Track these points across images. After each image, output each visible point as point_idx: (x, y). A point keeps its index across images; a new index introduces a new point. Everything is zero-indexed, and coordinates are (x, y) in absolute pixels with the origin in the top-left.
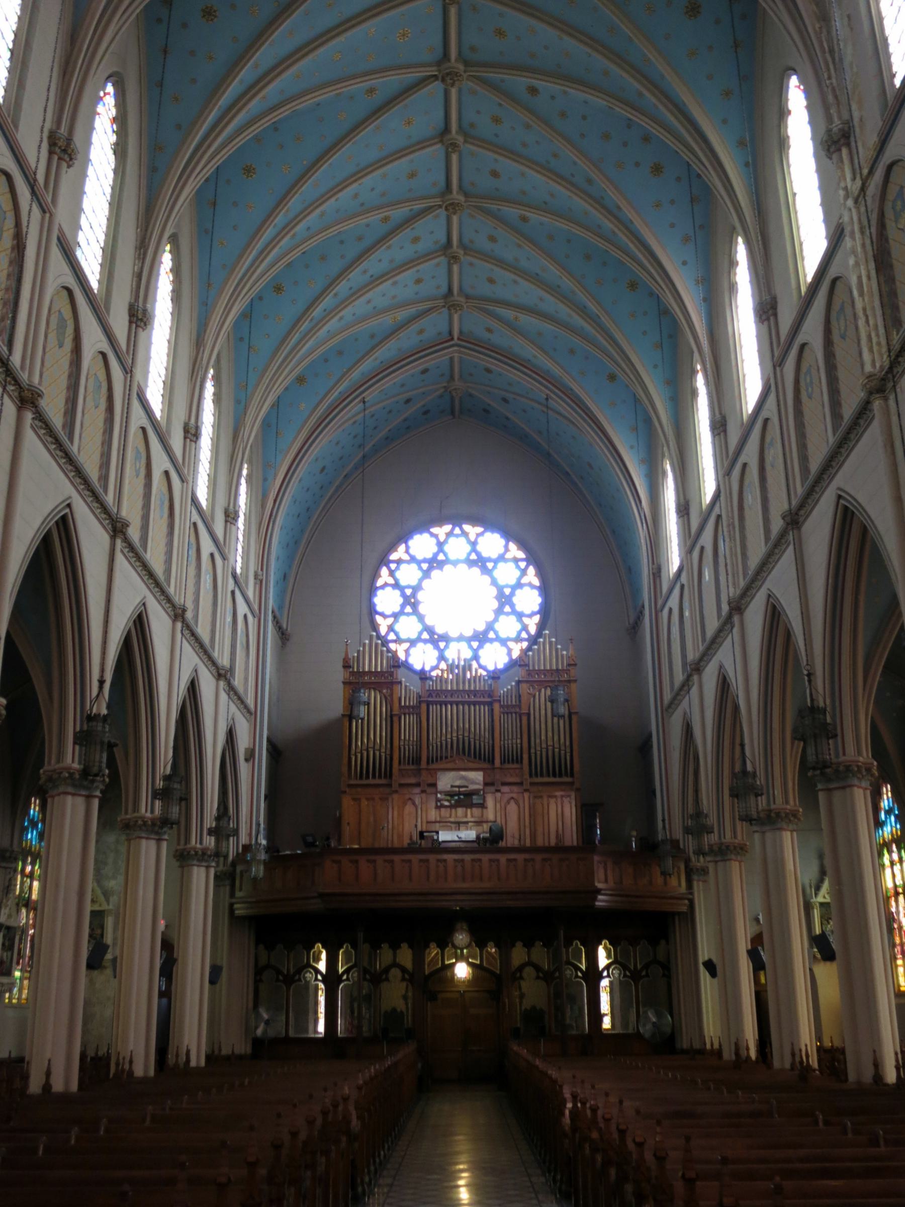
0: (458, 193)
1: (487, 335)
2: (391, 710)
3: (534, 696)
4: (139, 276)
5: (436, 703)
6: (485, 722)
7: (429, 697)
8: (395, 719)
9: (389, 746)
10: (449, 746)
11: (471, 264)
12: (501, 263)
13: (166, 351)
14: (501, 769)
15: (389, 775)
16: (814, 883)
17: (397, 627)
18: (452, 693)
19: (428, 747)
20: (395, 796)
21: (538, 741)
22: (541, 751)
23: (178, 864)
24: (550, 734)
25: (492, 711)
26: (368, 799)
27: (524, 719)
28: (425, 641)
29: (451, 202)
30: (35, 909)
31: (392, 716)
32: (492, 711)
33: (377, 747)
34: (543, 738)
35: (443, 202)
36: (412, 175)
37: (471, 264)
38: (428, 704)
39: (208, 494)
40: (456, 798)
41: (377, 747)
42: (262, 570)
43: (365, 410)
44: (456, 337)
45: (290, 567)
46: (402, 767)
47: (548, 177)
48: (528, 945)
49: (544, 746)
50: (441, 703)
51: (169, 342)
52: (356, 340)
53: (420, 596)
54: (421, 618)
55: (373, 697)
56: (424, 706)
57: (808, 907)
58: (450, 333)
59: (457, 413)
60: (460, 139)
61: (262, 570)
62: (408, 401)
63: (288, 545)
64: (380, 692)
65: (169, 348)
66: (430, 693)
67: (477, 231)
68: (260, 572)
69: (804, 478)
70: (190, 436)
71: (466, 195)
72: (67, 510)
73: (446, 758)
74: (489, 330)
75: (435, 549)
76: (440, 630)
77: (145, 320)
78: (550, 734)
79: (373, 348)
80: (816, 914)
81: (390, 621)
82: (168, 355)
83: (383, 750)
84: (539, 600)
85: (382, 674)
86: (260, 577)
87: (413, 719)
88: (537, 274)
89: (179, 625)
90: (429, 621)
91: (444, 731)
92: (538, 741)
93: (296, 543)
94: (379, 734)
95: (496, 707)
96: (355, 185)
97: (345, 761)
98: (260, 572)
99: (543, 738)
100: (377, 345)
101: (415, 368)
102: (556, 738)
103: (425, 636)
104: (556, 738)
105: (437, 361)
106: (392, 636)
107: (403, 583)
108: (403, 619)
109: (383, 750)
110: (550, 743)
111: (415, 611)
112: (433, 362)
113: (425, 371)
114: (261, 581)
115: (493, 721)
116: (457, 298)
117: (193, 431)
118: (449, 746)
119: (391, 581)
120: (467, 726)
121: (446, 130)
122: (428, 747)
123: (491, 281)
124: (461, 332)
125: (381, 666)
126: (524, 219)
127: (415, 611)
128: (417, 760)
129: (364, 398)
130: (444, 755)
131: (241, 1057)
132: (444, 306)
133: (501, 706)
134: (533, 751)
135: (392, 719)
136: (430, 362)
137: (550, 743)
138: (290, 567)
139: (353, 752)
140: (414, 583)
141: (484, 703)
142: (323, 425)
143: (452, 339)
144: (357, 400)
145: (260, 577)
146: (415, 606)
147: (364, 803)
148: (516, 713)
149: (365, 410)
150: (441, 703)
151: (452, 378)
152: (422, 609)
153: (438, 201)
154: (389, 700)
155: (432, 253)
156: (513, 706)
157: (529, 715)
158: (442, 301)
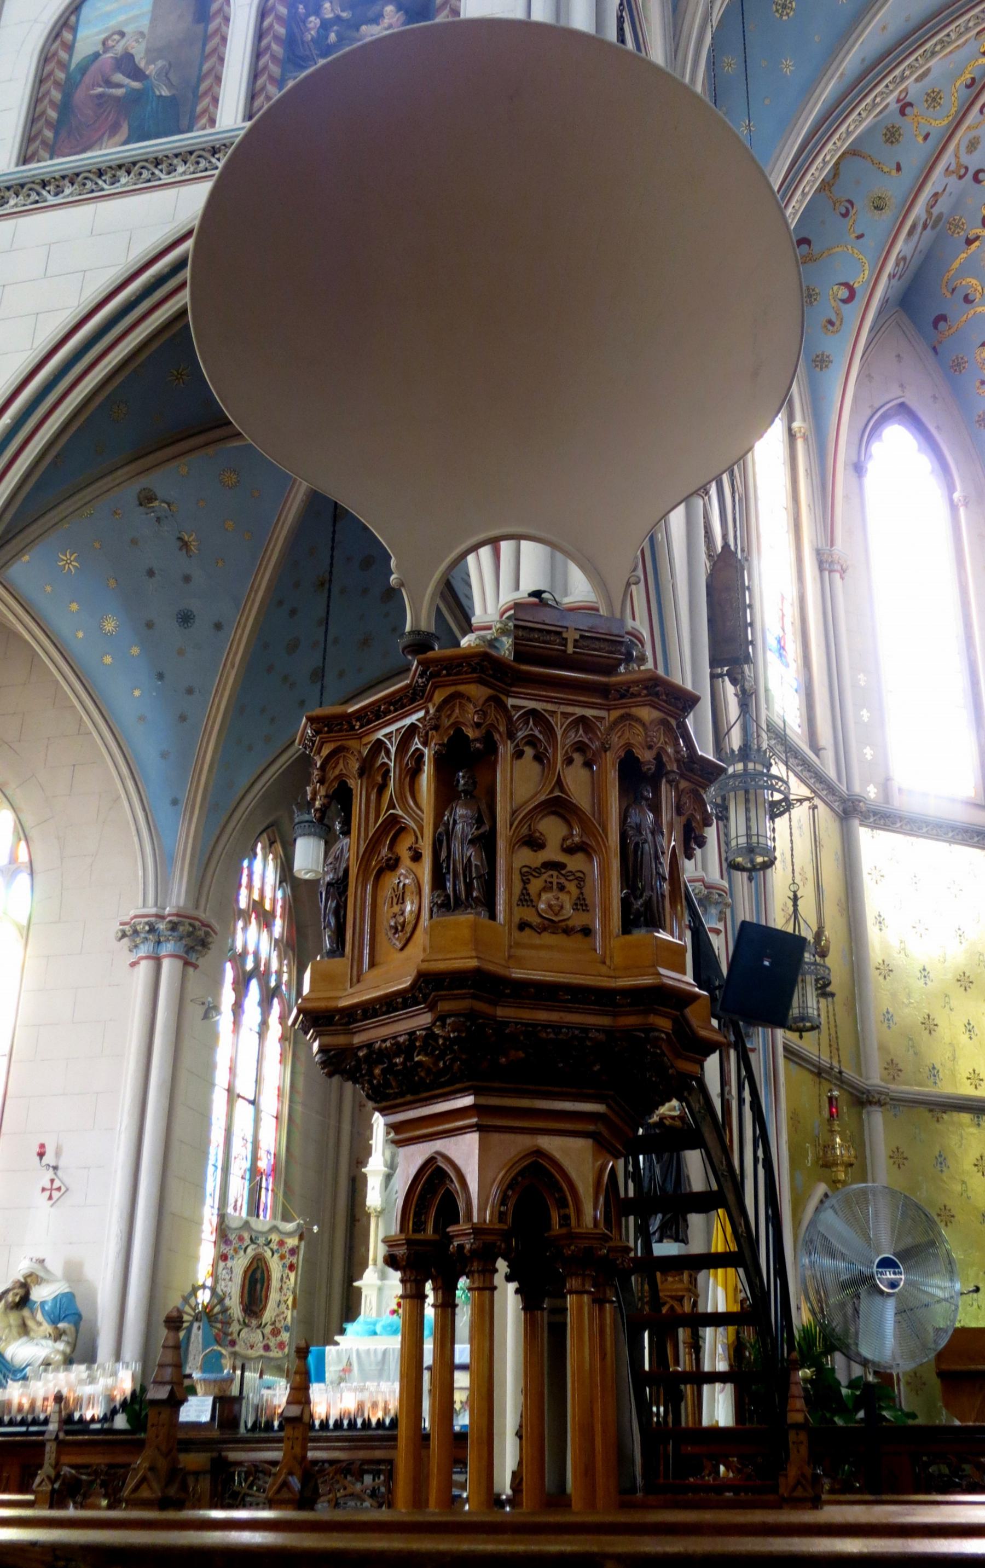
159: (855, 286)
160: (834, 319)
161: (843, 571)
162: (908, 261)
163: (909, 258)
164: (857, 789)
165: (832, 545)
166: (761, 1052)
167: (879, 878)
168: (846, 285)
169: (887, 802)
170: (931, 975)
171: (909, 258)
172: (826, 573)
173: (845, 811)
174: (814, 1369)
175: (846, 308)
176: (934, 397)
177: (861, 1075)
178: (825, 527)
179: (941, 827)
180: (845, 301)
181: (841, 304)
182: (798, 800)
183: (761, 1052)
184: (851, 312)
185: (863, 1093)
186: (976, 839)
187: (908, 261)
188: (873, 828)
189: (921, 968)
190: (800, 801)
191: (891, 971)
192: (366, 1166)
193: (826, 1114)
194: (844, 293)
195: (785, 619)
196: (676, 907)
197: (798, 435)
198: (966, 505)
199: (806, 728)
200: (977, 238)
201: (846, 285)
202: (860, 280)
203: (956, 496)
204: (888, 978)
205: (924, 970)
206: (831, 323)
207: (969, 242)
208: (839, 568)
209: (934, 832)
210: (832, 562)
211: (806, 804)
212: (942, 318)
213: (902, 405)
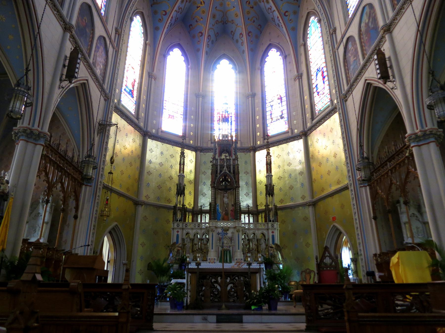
69: (348, 84)
72: (86, 82)
89: (68, 35)
159: (167, 12)
160: (161, 19)
161: (155, 79)
162: (183, 9)
163: (183, 8)
164: (149, 129)
165: (153, 72)
166: (93, 187)
167: (151, 150)
168: (165, 11)
169: (157, 134)
170: (162, 176)
171: (183, 8)
172: (150, 78)
173: (144, 134)
174: (16, 263)
175: (164, 17)
176: (188, 43)
177: (138, 198)
178: (152, 68)
179: (177, 143)
180: (164, 15)
181: (163, 15)
182: (113, 125)
183: (93, 187)
184: (165, 18)
185: (137, 202)
186: (180, 145)
187: (183, 9)
188: (152, 140)
189: (160, 174)
190: (114, 125)
191: (307, 218)
192: (346, 267)
193: (105, 203)
194: (164, 13)
195: (135, 86)
196: (59, 143)
197: (148, 44)
198: (191, 69)
199: (136, 113)
200: (199, 7)
201: (165, 11)
202: (168, 11)
203: (147, 42)
204: (150, 175)
205: (160, 174)
206: (160, 20)
207: (198, 7)
208: (154, 77)
209: (162, 140)
210: (152, 76)
211: (115, 126)
212: (191, 25)
213: (179, 44)
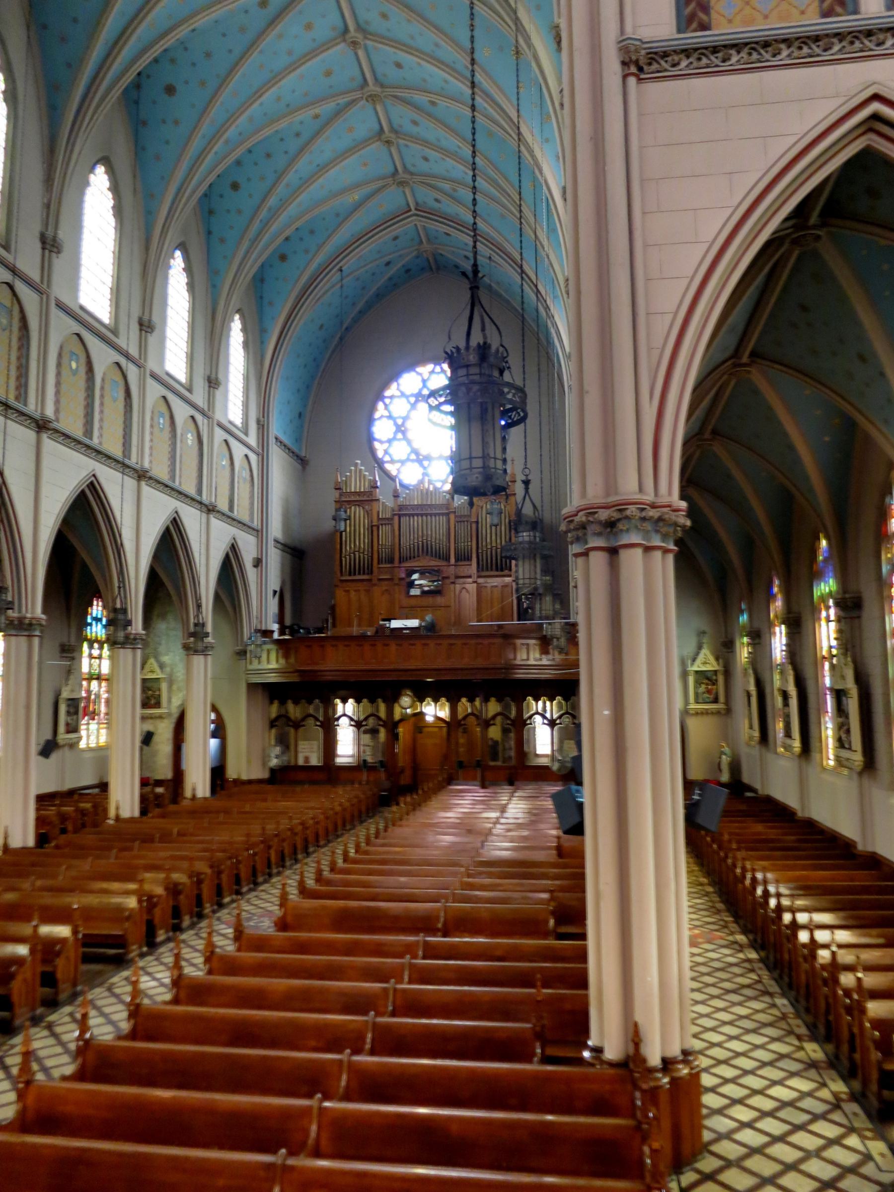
0: (374, 85)
1: (436, 205)
2: (372, 522)
3: (482, 508)
4: (48, 206)
5: (405, 515)
6: (444, 530)
7: (400, 510)
8: (375, 529)
9: (370, 550)
10: (420, 548)
11: (407, 146)
12: (426, 143)
13: (111, 261)
14: (455, 565)
15: (371, 572)
16: (692, 654)
17: (391, 451)
18: (414, 507)
19: (400, 550)
20: (375, 588)
21: (484, 543)
22: (487, 551)
23: (185, 652)
24: (494, 537)
25: (449, 521)
26: (355, 591)
27: (474, 526)
28: (413, 461)
29: (369, 93)
30: (106, 680)
31: (372, 526)
32: (449, 521)
33: (362, 551)
34: (488, 540)
35: (363, 94)
36: (328, 74)
37: (407, 146)
38: (400, 516)
39: (186, 368)
40: (435, 583)
41: (362, 551)
42: (263, 417)
43: (342, 280)
44: (413, 208)
45: (305, 406)
46: (380, 566)
47: (232, 123)
48: (471, 700)
49: (489, 547)
50: (409, 515)
51: (114, 253)
52: (324, 219)
53: (409, 424)
54: (409, 442)
55: (357, 512)
56: (396, 518)
57: (684, 674)
58: (408, 205)
59: (434, 270)
60: (359, 37)
61: (263, 417)
62: (388, 264)
63: (298, 390)
64: (363, 508)
65: (114, 259)
66: (401, 507)
67: (401, 117)
68: (262, 419)
70: (144, 328)
71: (382, 86)
73: (414, 557)
74: (437, 200)
75: (421, 385)
76: (424, 452)
77: (56, 245)
78: (494, 537)
79: (340, 224)
80: (691, 680)
81: (386, 446)
82: (113, 264)
83: (366, 553)
84: (453, 443)
85: (364, 493)
86: (262, 423)
87: (388, 528)
88: (456, 152)
90: (416, 445)
91: (412, 538)
92: (484, 543)
93: (308, 387)
94: (363, 542)
95: (452, 517)
96: (274, 89)
97: (338, 562)
98: (262, 419)
99: (488, 540)
100: (343, 221)
101: (385, 236)
102: (499, 541)
103: (413, 457)
104: (499, 541)
105: (405, 228)
106: (387, 458)
107: (395, 415)
108: (395, 443)
109: (366, 553)
110: (494, 544)
111: (405, 438)
112: (402, 229)
113: (395, 238)
114: (263, 426)
115: (449, 529)
116: (402, 175)
117: (146, 324)
118: (420, 548)
119: (386, 413)
120: (429, 533)
121: (346, 30)
122: (400, 550)
123: (426, 159)
124: (417, 204)
125: (364, 487)
126: (433, 103)
127: (405, 438)
128: (391, 560)
129: (341, 267)
130: (412, 555)
131: (260, 781)
132: (394, 183)
133: (456, 517)
134: (480, 551)
135: (373, 529)
136: (397, 230)
137: (494, 544)
138: (305, 406)
139: (343, 555)
140: (404, 414)
141: (443, 514)
142: (308, 293)
143: (410, 210)
144: (335, 270)
145: (262, 423)
146: (404, 433)
147: (353, 594)
148: (467, 521)
149: (342, 280)
150: (409, 515)
151: (421, 242)
152: (410, 435)
153: (358, 95)
154: (368, 513)
155: (370, 139)
156: (465, 516)
157: (477, 522)
158: (391, 179)
